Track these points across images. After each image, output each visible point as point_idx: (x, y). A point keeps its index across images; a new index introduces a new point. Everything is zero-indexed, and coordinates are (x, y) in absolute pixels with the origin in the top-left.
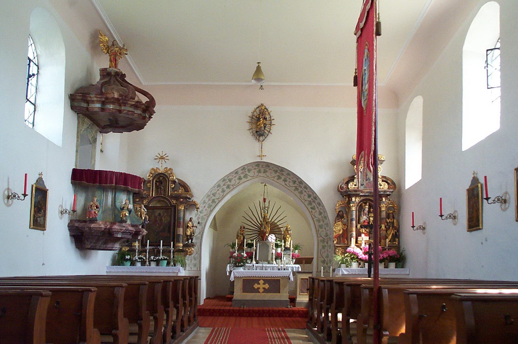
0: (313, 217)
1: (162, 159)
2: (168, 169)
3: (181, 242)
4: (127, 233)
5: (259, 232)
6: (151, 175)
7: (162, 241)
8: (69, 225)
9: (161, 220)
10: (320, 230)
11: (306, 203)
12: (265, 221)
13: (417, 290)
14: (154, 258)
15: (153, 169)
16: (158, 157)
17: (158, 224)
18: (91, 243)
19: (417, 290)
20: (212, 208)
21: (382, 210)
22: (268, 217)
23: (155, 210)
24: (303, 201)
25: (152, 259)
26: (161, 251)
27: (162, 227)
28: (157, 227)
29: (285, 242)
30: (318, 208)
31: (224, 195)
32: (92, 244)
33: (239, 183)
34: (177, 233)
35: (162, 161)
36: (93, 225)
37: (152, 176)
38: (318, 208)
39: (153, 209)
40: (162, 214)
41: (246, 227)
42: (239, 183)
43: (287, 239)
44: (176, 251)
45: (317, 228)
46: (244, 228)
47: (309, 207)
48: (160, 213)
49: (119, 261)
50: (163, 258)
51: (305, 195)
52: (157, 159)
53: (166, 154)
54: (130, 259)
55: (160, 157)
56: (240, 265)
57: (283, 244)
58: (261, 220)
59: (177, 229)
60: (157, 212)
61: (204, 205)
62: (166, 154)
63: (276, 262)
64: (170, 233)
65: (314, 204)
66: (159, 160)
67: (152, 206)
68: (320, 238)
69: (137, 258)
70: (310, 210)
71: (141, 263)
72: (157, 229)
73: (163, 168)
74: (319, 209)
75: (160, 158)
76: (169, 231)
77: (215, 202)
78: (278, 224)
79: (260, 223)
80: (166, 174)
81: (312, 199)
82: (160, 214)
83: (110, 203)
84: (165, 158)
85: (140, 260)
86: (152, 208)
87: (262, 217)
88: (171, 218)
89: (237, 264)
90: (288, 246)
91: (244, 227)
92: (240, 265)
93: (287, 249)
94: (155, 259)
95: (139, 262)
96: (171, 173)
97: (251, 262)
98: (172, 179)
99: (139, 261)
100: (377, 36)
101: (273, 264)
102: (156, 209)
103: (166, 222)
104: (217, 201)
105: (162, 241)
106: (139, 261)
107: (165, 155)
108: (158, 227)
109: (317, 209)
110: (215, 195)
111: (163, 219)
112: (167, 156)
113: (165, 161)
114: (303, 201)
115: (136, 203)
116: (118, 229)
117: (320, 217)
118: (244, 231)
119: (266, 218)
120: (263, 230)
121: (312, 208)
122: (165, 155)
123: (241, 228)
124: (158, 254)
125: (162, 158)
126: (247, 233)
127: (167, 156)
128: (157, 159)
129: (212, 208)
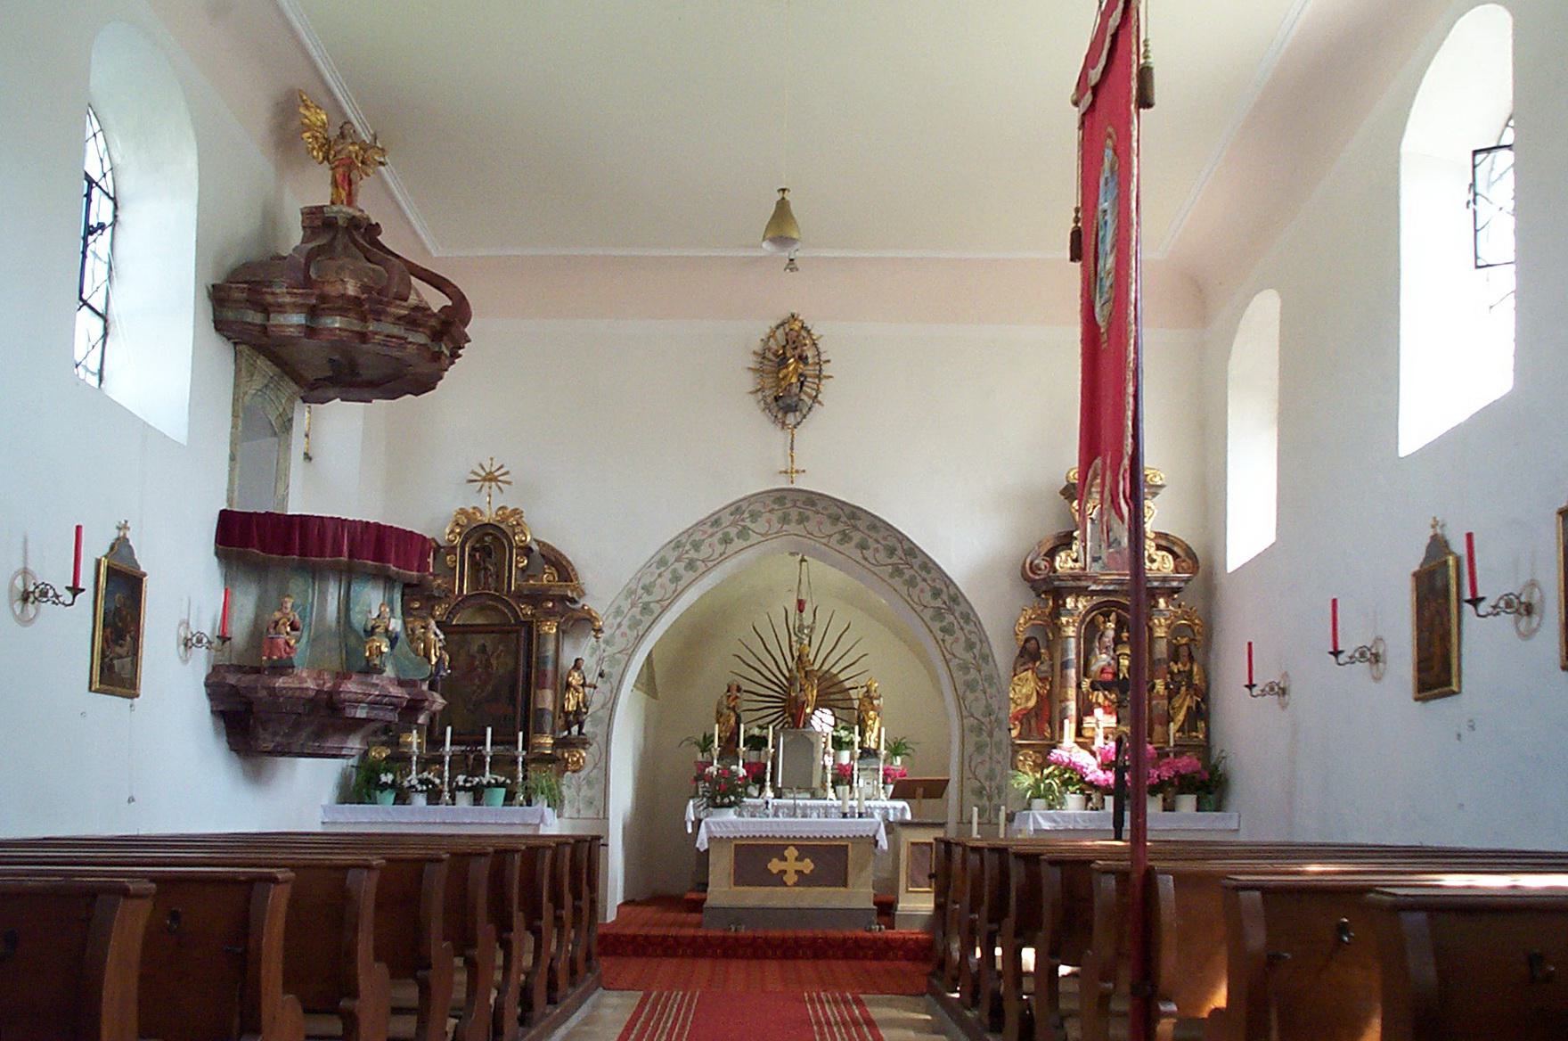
0: (948, 656)
1: (490, 480)
2: (508, 512)
3: (548, 731)
4: (386, 704)
5: (784, 701)
6: (458, 530)
7: (489, 730)
8: (210, 681)
9: (488, 665)
10: (970, 696)
11: (928, 614)
12: (804, 668)
13: (1263, 878)
14: (466, 781)
15: (463, 512)
16: (480, 476)
17: (480, 678)
18: (275, 734)
19: (1263, 878)
20: (641, 629)
21: (1157, 635)
22: (811, 657)
23: (469, 637)
24: (919, 608)
25: (461, 783)
26: (488, 759)
27: (489, 688)
28: (475, 688)
29: (862, 733)
30: (962, 629)
31: (679, 589)
32: (278, 739)
33: (724, 553)
34: (535, 704)
35: (490, 488)
36: (281, 680)
37: (460, 534)
38: (962, 629)
39: (464, 633)
40: (489, 649)
41: (746, 685)
42: (724, 553)
43: (870, 722)
44: (533, 760)
45: (961, 689)
46: (739, 689)
47: (936, 626)
48: (484, 646)
49: (359, 789)
50: (493, 781)
51: (922, 591)
52: (475, 481)
53: (502, 467)
54: (393, 785)
55: (484, 474)
56: (726, 800)
57: (857, 739)
58: (790, 664)
59: (535, 693)
60: (477, 641)
61: (619, 619)
62: (502, 467)
63: (835, 791)
64: (514, 706)
65: (949, 618)
66: (480, 484)
67: (461, 623)
68: (969, 722)
69: (414, 782)
70: (940, 635)
71: (425, 794)
72: (475, 692)
73: (495, 508)
74: (966, 631)
75: (484, 480)
76: (512, 699)
77: (652, 612)
78: (842, 677)
79: (787, 675)
80: (502, 526)
81: (945, 603)
82: (483, 649)
83: (334, 614)
84: (500, 478)
85: (425, 788)
86: (461, 629)
87: (793, 658)
88: (517, 658)
89: (719, 798)
90: (873, 746)
91: (738, 687)
92: (726, 800)
93: (867, 753)
94: (468, 785)
95: (422, 791)
96: (518, 524)
97: (760, 794)
98: (522, 541)
99: (420, 789)
100: (1141, 110)
101: (825, 799)
102: (473, 632)
103: (501, 671)
104: (656, 608)
105: (489, 730)
106: (420, 789)
107: (498, 469)
108: (478, 687)
109: (959, 633)
110: (651, 589)
111: (494, 662)
112: (507, 473)
113: (500, 488)
114: (919, 608)
115: (411, 615)
116: (356, 693)
117: (968, 656)
118: (738, 701)
119: (805, 659)
120: (796, 696)
121: (943, 630)
122: (498, 469)
123: (728, 691)
124: (478, 768)
125: (490, 478)
126: (746, 705)
127: (507, 473)
128: (475, 481)
129: (641, 629)
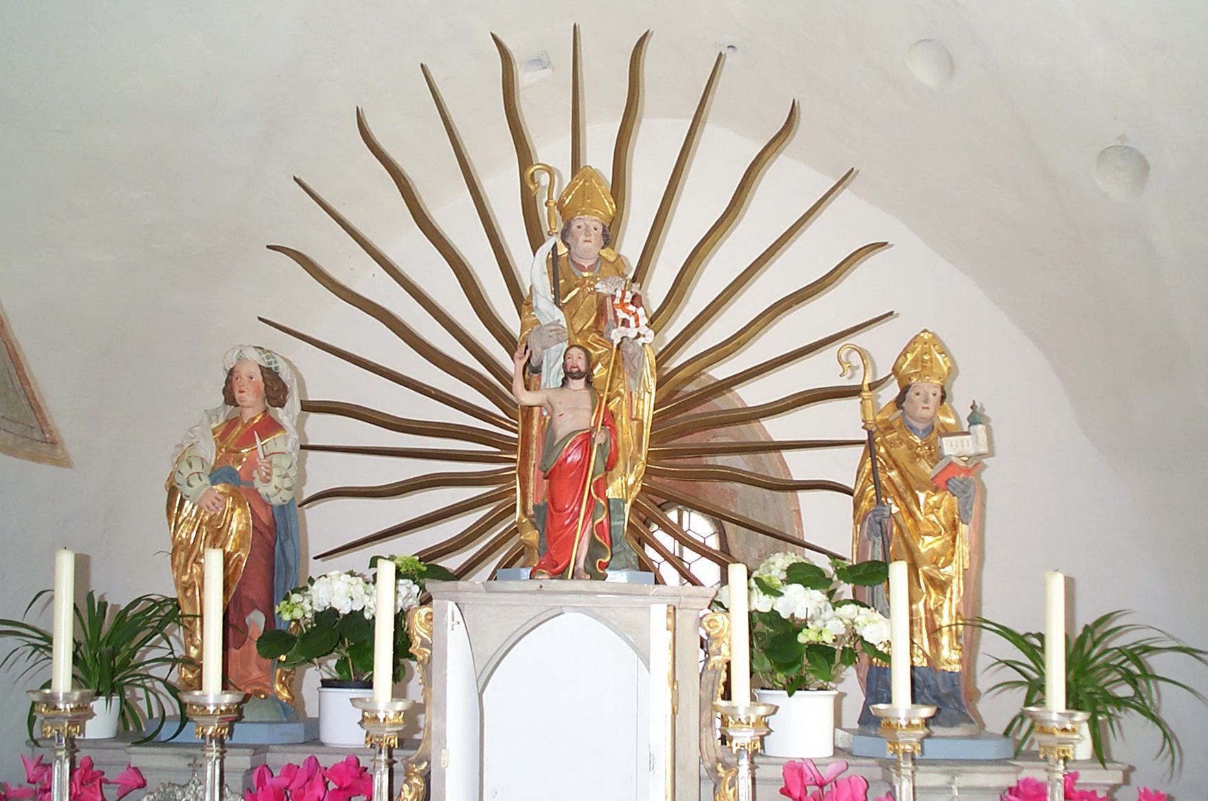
5: (505, 445)
22: (631, 247)
87: (536, 240)
